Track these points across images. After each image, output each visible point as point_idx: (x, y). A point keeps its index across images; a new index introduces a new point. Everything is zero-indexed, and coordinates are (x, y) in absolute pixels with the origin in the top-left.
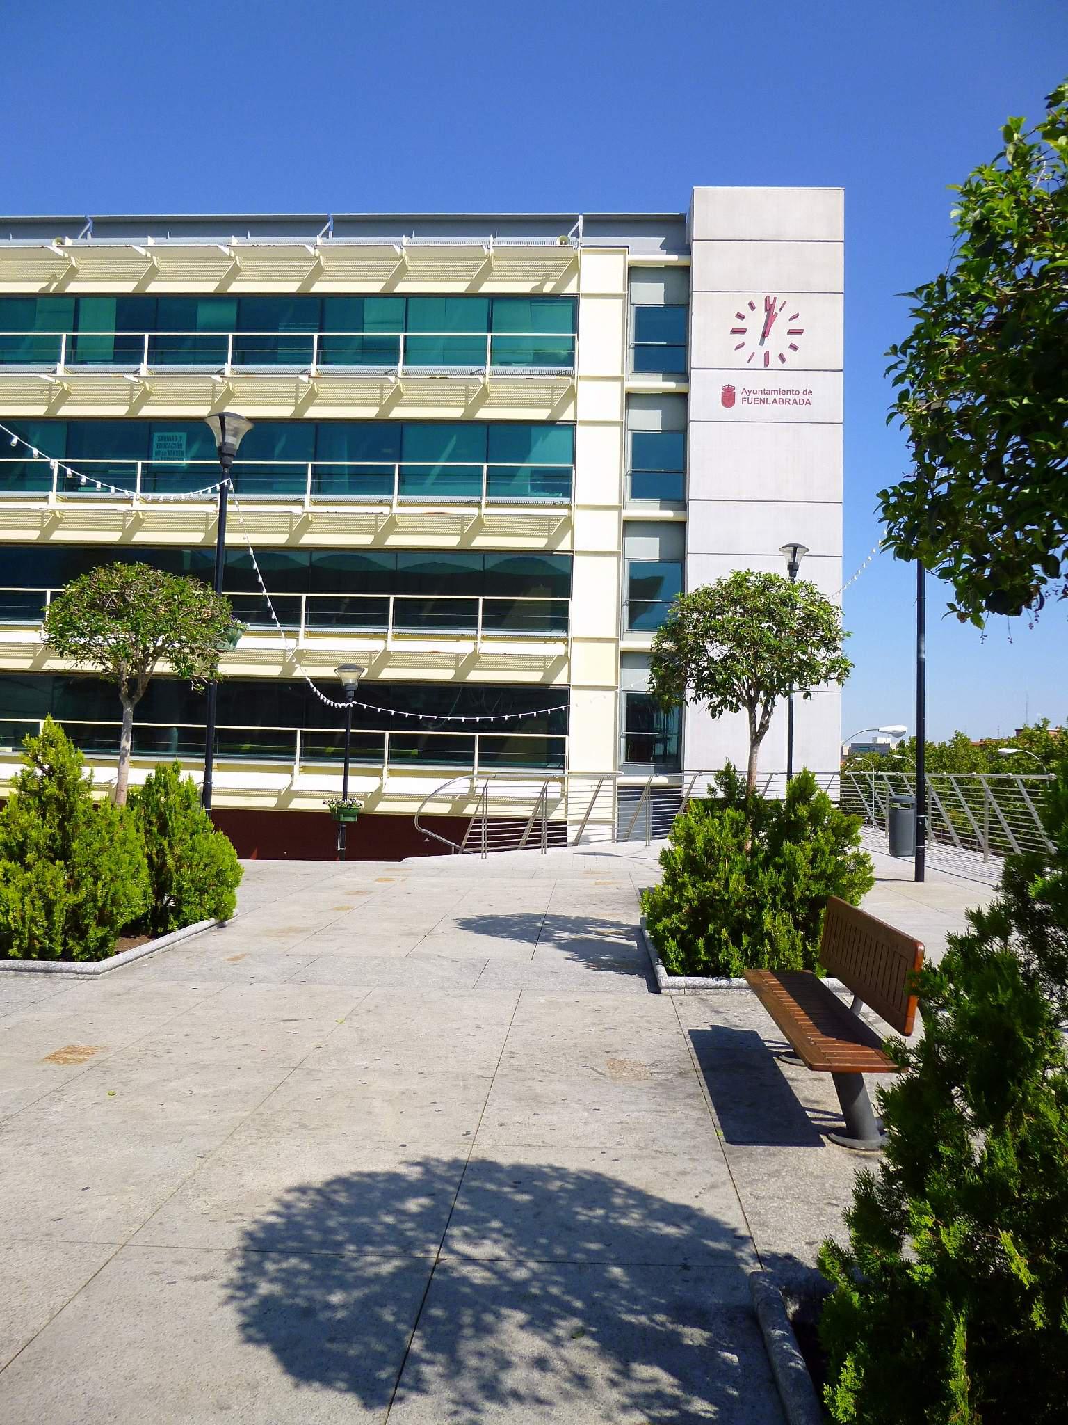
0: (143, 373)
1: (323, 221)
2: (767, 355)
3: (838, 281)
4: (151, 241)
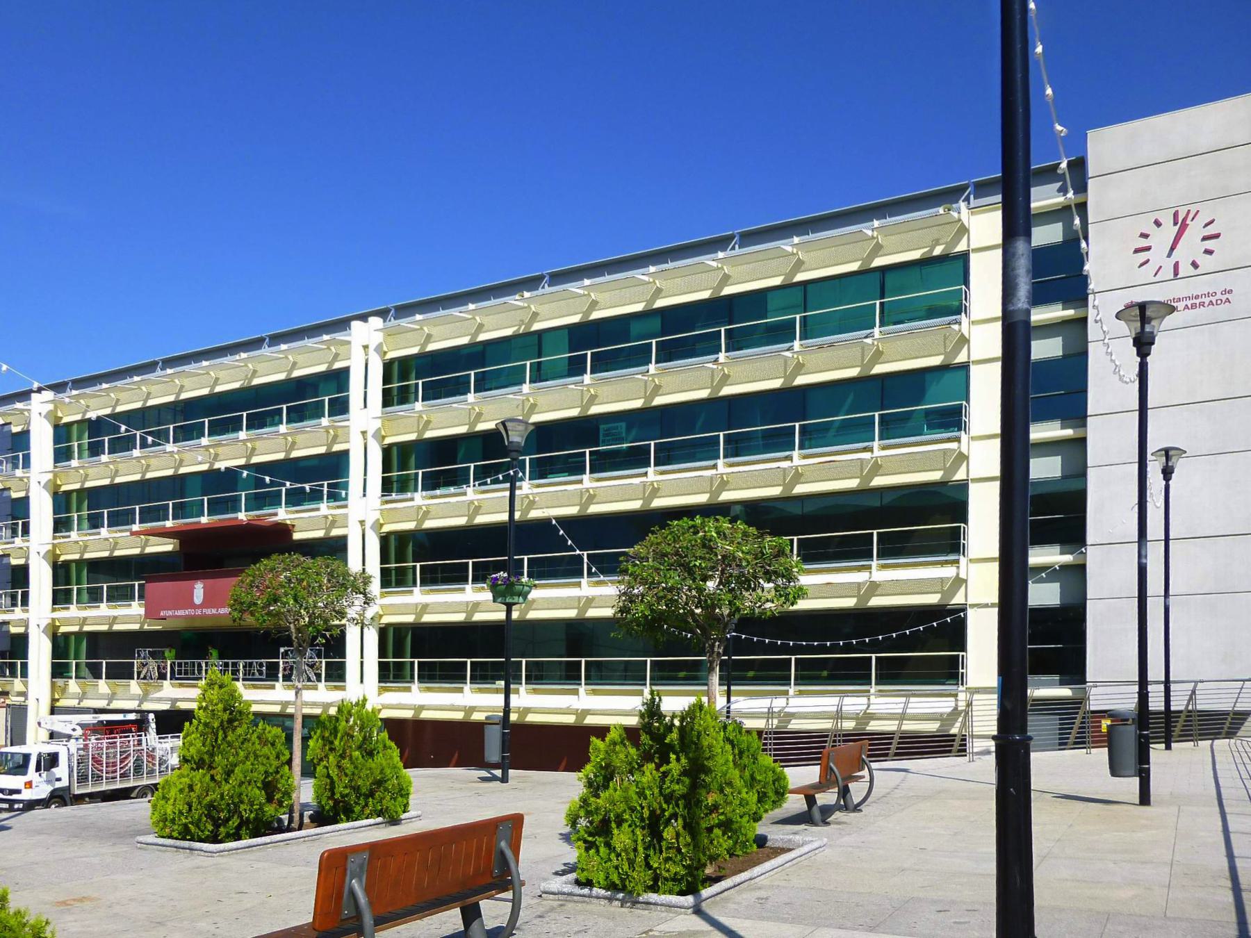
0: (877, 335)
1: (731, 238)
2: (1176, 266)
4: (796, 240)
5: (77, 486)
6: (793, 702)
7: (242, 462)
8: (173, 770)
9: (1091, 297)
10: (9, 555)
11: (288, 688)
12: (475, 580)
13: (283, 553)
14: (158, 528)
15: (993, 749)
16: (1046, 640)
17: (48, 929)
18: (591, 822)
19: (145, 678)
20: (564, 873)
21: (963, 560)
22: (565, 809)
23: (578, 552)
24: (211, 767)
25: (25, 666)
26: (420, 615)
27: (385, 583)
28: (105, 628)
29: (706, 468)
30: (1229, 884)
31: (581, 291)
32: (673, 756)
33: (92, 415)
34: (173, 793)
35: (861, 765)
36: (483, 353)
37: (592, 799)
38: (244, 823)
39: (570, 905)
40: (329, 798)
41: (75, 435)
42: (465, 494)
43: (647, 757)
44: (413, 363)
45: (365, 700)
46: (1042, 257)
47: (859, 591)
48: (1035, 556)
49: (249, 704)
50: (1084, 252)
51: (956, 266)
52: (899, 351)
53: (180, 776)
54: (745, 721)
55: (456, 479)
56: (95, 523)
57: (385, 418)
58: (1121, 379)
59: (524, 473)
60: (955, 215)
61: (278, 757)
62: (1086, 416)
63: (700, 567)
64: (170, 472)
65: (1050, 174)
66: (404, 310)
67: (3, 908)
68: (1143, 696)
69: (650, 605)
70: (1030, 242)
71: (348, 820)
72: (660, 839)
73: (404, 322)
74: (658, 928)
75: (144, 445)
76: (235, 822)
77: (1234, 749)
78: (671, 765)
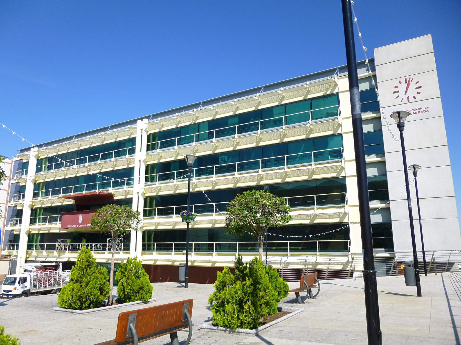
0: (310, 123)
1: (261, 88)
2: (408, 98)
3: (433, 66)
4: (282, 89)
5: (42, 181)
6: (289, 258)
7: (98, 171)
8: (67, 283)
9: (381, 109)
10: (17, 206)
11: (110, 253)
12: (176, 213)
13: (110, 204)
14: (69, 196)
15: (363, 276)
16: (378, 236)
17: (18, 342)
18: (218, 303)
19: (59, 250)
20: (208, 321)
21: (346, 206)
22: (208, 297)
23: (212, 203)
24: (81, 282)
25: (18, 246)
26: (174, 226)
27: (145, 215)
28: (47, 232)
29: (255, 172)
30: (452, 325)
31: (212, 108)
32: (247, 278)
33: (50, 156)
34: (67, 292)
35: (315, 281)
36: (180, 131)
37: (218, 294)
38: (91, 302)
39: (210, 333)
40: (123, 294)
41: (44, 163)
42: (173, 182)
43: (238, 278)
44: (157, 135)
45: (137, 258)
46: (363, 94)
47: (311, 217)
48: (372, 204)
49: (95, 259)
50: (377, 93)
51: (334, 98)
52: (318, 129)
53: (69, 286)
54: (272, 265)
55: (169, 177)
56: (47, 194)
57: (147, 155)
58: (395, 139)
59: (193, 174)
60: (333, 79)
61: (105, 279)
62: (384, 153)
63: (255, 209)
64: (74, 176)
65: (362, 64)
66: (155, 116)
67: (2, 334)
68: (415, 257)
69: (237, 223)
70: (358, 89)
71: (129, 302)
72: (243, 308)
73: (155, 121)
74: (242, 341)
75: (66, 166)
76: (88, 302)
77: (450, 276)
78: (246, 282)
